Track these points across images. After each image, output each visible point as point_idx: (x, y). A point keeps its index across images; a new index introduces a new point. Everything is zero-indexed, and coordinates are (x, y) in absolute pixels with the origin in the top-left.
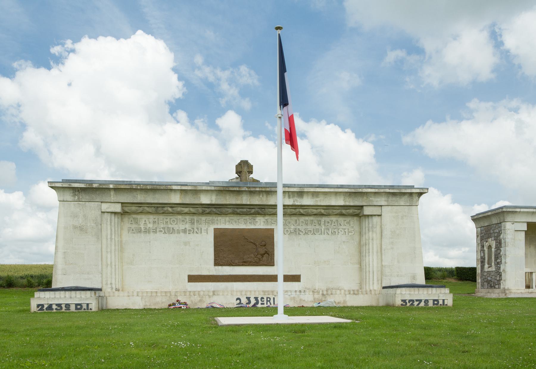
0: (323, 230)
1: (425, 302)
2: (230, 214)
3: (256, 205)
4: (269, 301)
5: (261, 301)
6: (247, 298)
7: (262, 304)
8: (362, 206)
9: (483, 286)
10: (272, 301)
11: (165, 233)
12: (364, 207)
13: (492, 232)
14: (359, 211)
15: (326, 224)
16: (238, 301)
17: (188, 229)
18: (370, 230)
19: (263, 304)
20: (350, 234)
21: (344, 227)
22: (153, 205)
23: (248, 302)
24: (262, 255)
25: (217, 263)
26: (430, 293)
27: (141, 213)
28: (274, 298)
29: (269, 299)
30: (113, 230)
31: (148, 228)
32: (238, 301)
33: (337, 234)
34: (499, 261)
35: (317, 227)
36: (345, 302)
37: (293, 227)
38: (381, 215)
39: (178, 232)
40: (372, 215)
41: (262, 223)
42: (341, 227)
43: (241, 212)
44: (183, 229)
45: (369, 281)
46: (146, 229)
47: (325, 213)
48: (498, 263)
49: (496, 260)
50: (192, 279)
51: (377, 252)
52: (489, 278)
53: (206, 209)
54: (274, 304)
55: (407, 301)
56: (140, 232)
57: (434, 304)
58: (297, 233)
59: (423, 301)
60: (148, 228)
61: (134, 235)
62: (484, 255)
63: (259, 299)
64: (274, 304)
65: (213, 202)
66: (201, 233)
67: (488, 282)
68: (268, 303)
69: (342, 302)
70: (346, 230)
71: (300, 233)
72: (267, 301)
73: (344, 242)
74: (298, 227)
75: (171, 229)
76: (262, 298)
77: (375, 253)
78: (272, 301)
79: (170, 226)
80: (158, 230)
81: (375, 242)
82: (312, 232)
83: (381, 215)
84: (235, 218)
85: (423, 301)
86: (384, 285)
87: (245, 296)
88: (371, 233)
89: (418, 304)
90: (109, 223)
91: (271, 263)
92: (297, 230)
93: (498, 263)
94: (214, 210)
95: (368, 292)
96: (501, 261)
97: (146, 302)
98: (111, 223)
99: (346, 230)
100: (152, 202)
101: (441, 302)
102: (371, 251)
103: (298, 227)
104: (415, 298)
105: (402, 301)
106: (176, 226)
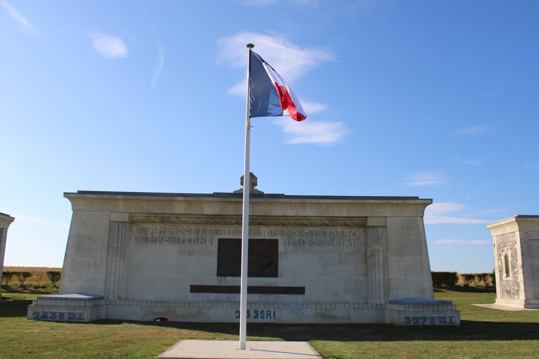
0: (328, 241)
1: (430, 320)
2: (234, 224)
3: (259, 216)
4: (270, 315)
5: (261, 314)
7: (261, 318)
8: (367, 217)
9: (502, 295)
10: (272, 315)
11: (170, 242)
12: (368, 219)
13: (507, 241)
15: (332, 235)
17: (193, 239)
19: (263, 318)
20: (356, 245)
21: (350, 238)
22: (159, 215)
25: (221, 273)
26: (436, 309)
27: (148, 222)
28: (274, 312)
30: (120, 239)
34: (516, 270)
36: (349, 317)
37: (297, 238)
38: (386, 226)
40: (373, 227)
41: (266, 234)
47: (330, 224)
48: (515, 273)
49: (513, 269)
50: (195, 289)
52: (508, 288)
53: (210, 220)
54: (274, 317)
55: (411, 319)
57: (441, 322)
58: (302, 244)
59: (429, 318)
62: (502, 264)
64: (274, 317)
65: (217, 213)
66: (205, 243)
67: (508, 292)
68: (269, 317)
72: (267, 315)
73: (350, 253)
74: (303, 238)
75: (177, 239)
76: (262, 312)
78: (272, 315)
79: (176, 235)
80: (164, 239)
82: (317, 243)
83: (386, 226)
85: (429, 318)
86: (391, 299)
89: (423, 322)
90: (116, 232)
91: (275, 274)
93: (515, 273)
94: (218, 220)
95: (374, 307)
96: (518, 271)
98: (118, 231)
99: (352, 242)
100: (158, 212)
101: (448, 320)
102: (377, 263)
103: (303, 238)
104: (419, 315)
105: (406, 318)
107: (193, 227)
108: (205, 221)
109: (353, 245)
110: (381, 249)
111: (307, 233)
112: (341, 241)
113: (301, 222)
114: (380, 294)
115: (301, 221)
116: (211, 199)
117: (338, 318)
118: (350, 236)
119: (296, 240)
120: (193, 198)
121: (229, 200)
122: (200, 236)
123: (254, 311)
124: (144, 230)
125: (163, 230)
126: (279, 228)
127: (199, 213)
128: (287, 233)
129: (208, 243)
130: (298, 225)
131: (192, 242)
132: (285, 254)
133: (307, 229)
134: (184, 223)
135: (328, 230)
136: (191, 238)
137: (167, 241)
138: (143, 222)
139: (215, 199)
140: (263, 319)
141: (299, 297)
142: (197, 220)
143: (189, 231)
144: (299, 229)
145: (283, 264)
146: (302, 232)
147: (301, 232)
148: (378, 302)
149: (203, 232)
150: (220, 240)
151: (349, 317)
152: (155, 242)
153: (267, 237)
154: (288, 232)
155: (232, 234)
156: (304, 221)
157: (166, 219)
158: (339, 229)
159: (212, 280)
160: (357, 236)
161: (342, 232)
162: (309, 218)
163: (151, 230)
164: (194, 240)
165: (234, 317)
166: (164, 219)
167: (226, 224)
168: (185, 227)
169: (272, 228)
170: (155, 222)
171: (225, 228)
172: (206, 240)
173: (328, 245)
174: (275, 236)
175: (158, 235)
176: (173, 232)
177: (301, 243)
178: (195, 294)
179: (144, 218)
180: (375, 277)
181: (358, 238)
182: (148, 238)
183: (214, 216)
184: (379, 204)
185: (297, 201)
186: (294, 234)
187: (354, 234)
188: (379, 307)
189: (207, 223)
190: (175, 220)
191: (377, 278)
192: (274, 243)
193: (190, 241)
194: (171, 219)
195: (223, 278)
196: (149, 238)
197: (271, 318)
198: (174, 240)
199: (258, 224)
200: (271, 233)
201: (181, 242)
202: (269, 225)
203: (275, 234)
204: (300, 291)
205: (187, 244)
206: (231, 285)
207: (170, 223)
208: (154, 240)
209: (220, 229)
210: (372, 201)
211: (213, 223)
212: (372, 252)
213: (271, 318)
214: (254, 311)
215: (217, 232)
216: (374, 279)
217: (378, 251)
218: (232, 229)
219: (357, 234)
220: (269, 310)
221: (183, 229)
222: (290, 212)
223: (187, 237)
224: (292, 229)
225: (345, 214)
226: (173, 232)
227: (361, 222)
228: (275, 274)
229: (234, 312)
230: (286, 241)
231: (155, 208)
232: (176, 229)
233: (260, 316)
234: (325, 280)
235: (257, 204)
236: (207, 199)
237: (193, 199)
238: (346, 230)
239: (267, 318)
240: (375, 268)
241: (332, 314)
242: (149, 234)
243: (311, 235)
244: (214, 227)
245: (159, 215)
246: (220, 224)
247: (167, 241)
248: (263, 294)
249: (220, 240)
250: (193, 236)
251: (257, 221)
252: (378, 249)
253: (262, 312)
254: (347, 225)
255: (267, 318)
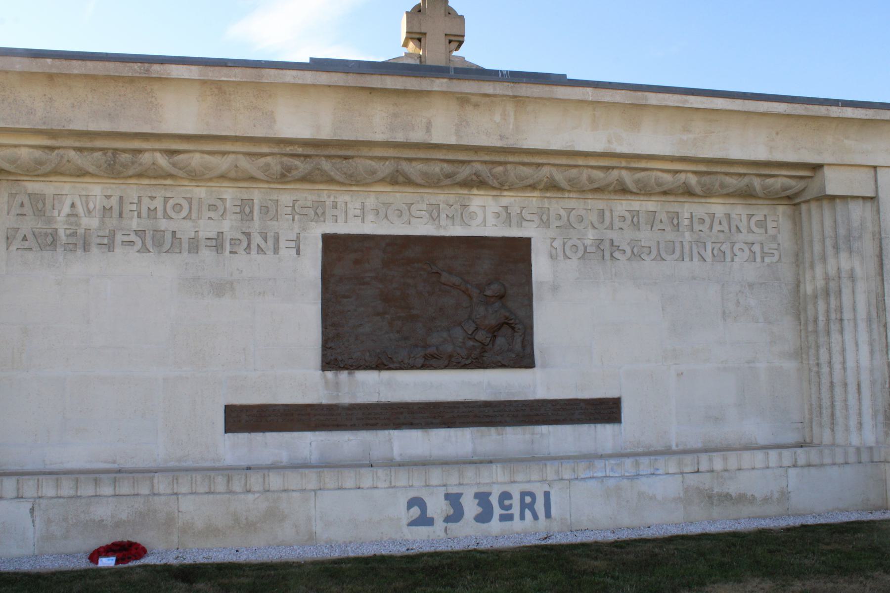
2: (382, 181)
3: (477, 149)
5: (502, 506)
6: (447, 496)
8: (817, 167)
10: (540, 506)
11: (144, 249)
14: (801, 184)
15: (697, 227)
16: (416, 511)
17: (228, 236)
18: (842, 245)
19: (510, 518)
21: (750, 238)
22: (99, 143)
23: (451, 512)
24: (494, 332)
25: (334, 359)
28: (547, 495)
29: (528, 499)
31: (81, 231)
32: (416, 511)
33: (728, 259)
35: (670, 235)
36: (784, 495)
37: (591, 235)
39: (194, 246)
40: (844, 198)
41: (491, 220)
42: (741, 237)
43: (425, 175)
44: (213, 235)
45: (847, 418)
46: (74, 234)
51: (869, 320)
53: (296, 162)
54: (548, 515)
56: (53, 243)
60: (81, 231)
61: (30, 256)
63: (494, 500)
64: (548, 515)
65: (325, 134)
66: (276, 250)
68: (528, 513)
69: (776, 495)
70: (756, 248)
71: (617, 254)
72: (523, 506)
73: (751, 286)
74: (610, 234)
75: (168, 236)
76: (505, 496)
77: (862, 326)
78: (540, 506)
79: (163, 224)
80: (119, 238)
81: (861, 286)
84: (400, 196)
87: (442, 491)
88: (843, 255)
91: (524, 359)
92: (606, 245)
94: (326, 165)
97: (49, 521)
99: (756, 248)
100: (93, 127)
102: (847, 315)
103: (610, 234)
106: (188, 224)
107: (230, 194)
108: (276, 168)
109: (758, 259)
110: (859, 272)
111: (623, 218)
112: (726, 247)
113: (614, 177)
114: (860, 414)
115: (615, 173)
116: (309, 77)
117: (752, 500)
118: (750, 231)
119: (588, 242)
120: (238, 71)
121: (376, 81)
122: (256, 225)
123: (477, 495)
124: (39, 206)
125: (114, 202)
126: (533, 199)
127: (259, 132)
128: (560, 217)
129: (286, 253)
130: (599, 190)
131: (228, 247)
132: (555, 288)
133: (623, 206)
134: (195, 176)
135: (687, 209)
136: (220, 234)
137: (131, 243)
138: (36, 171)
139: (323, 78)
140: (508, 523)
141: (601, 436)
142: (244, 163)
143: (212, 207)
144: (596, 203)
145: (548, 322)
146: (607, 214)
147: (602, 213)
148: (855, 440)
149: (264, 210)
150: (331, 242)
151: (784, 495)
152: (86, 247)
153: (493, 229)
154: (563, 213)
155: (370, 217)
156: (624, 173)
157: (125, 157)
158: (718, 207)
159: (309, 385)
160: (771, 232)
161: (728, 216)
162: (643, 164)
163: (68, 203)
164: (234, 241)
165: (405, 522)
166: (118, 157)
167: (353, 180)
168: (200, 192)
169: (509, 199)
170: (82, 173)
171: (347, 198)
172: (277, 240)
173: (687, 259)
174: (520, 225)
175: (93, 223)
176: (152, 212)
177: (606, 251)
178: (242, 437)
179: (38, 154)
180: (844, 362)
181: (774, 238)
182: (54, 235)
183: (315, 146)
184: (865, 123)
185: (619, 96)
186: (581, 219)
187: (762, 224)
188: (865, 457)
189: (284, 177)
190: (162, 161)
191: (850, 364)
192: (517, 251)
193: (217, 243)
194: (146, 158)
195: (344, 375)
196: (61, 232)
197: (536, 517)
198: (158, 242)
199: (466, 184)
200: (507, 216)
201: (185, 246)
202: (501, 186)
203: (522, 219)
204: (606, 411)
205: (206, 254)
206: (373, 399)
207: (140, 175)
208: (82, 243)
209: (329, 202)
210: (849, 112)
211: (305, 179)
212: (827, 278)
213: (536, 517)
214: (477, 495)
215: (319, 213)
216: (837, 367)
217: (852, 277)
218: (371, 201)
219: (770, 224)
220: (527, 487)
221: (190, 200)
222: (587, 136)
223: (207, 229)
224: (573, 202)
225: (761, 154)
226: (152, 212)
227: (792, 182)
228: (524, 359)
229: (403, 502)
230: (555, 244)
231: (81, 111)
232: (166, 200)
233: (497, 511)
234: (680, 374)
235: (476, 105)
236: (290, 76)
237: (237, 75)
238: (739, 211)
239: (522, 517)
240: (841, 331)
241: (733, 488)
242: (61, 218)
243: (636, 226)
244: (306, 195)
245: (99, 143)
246: (331, 181)
247: (131, 243)
248: (484, 429)
249: (331, 242)
250: (228, 226)
251: (465, 172)
252: (852, 270)
253: (505, 496)
254: (747, 195)
255: (522, 517)
